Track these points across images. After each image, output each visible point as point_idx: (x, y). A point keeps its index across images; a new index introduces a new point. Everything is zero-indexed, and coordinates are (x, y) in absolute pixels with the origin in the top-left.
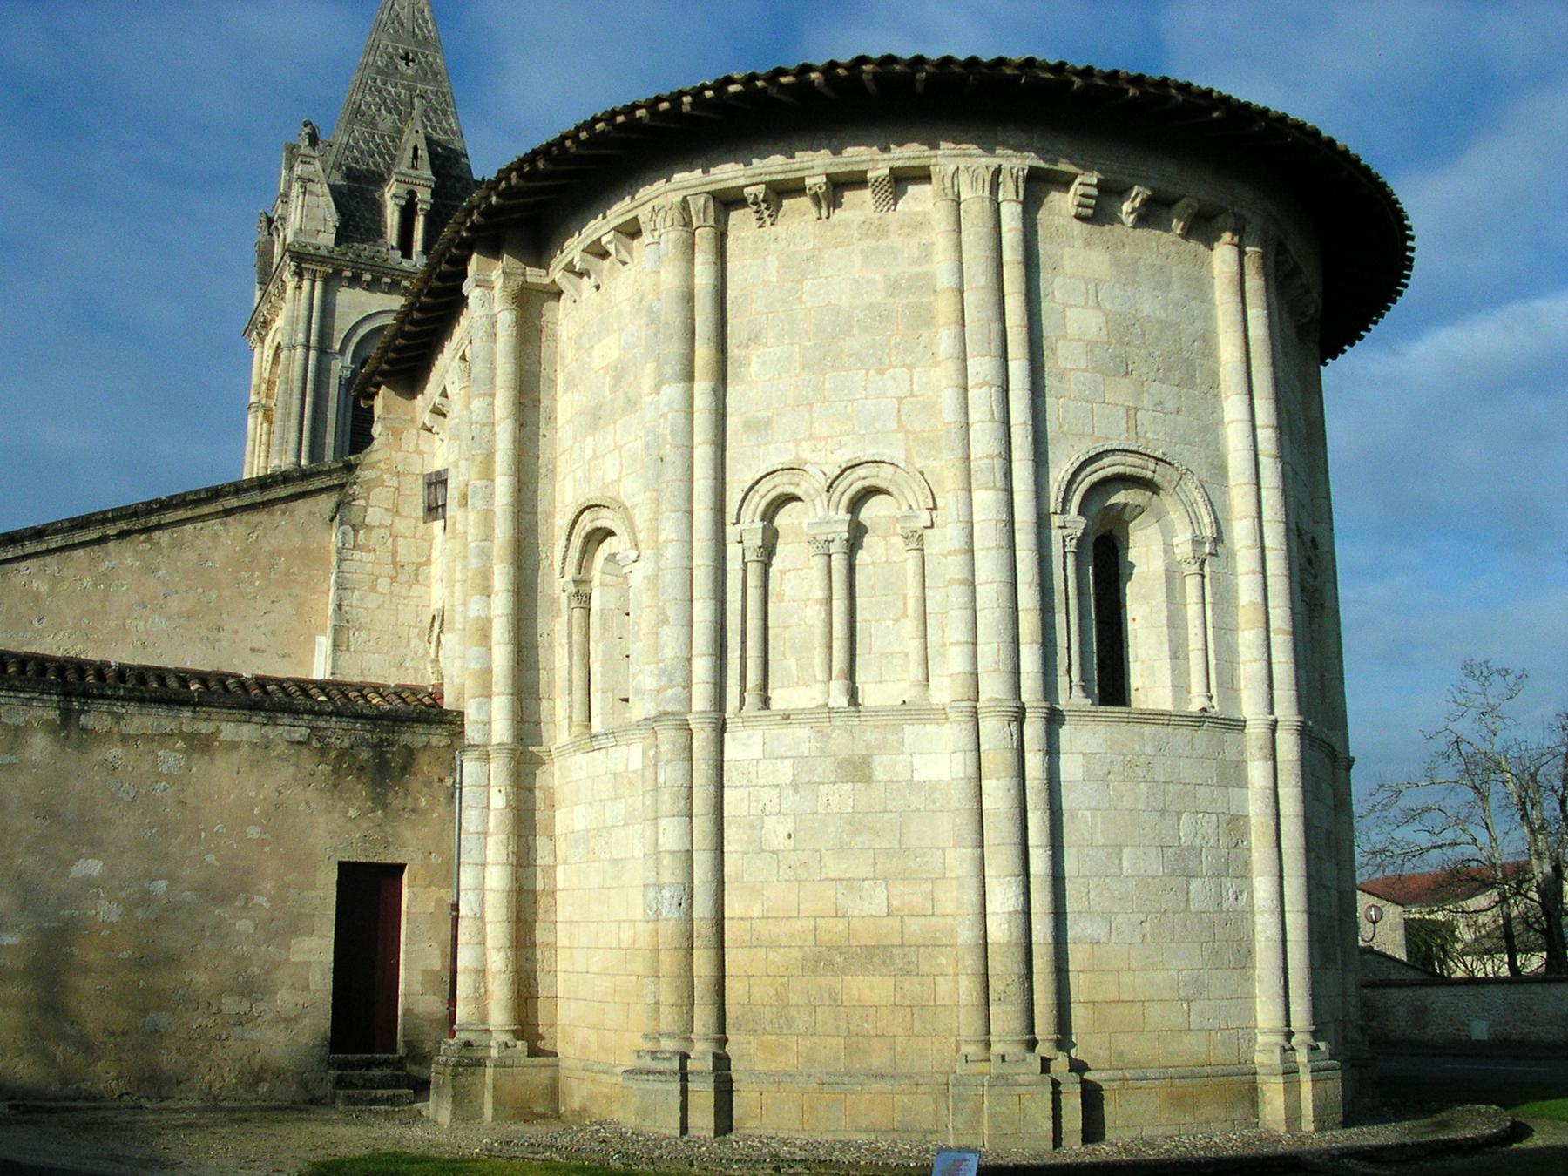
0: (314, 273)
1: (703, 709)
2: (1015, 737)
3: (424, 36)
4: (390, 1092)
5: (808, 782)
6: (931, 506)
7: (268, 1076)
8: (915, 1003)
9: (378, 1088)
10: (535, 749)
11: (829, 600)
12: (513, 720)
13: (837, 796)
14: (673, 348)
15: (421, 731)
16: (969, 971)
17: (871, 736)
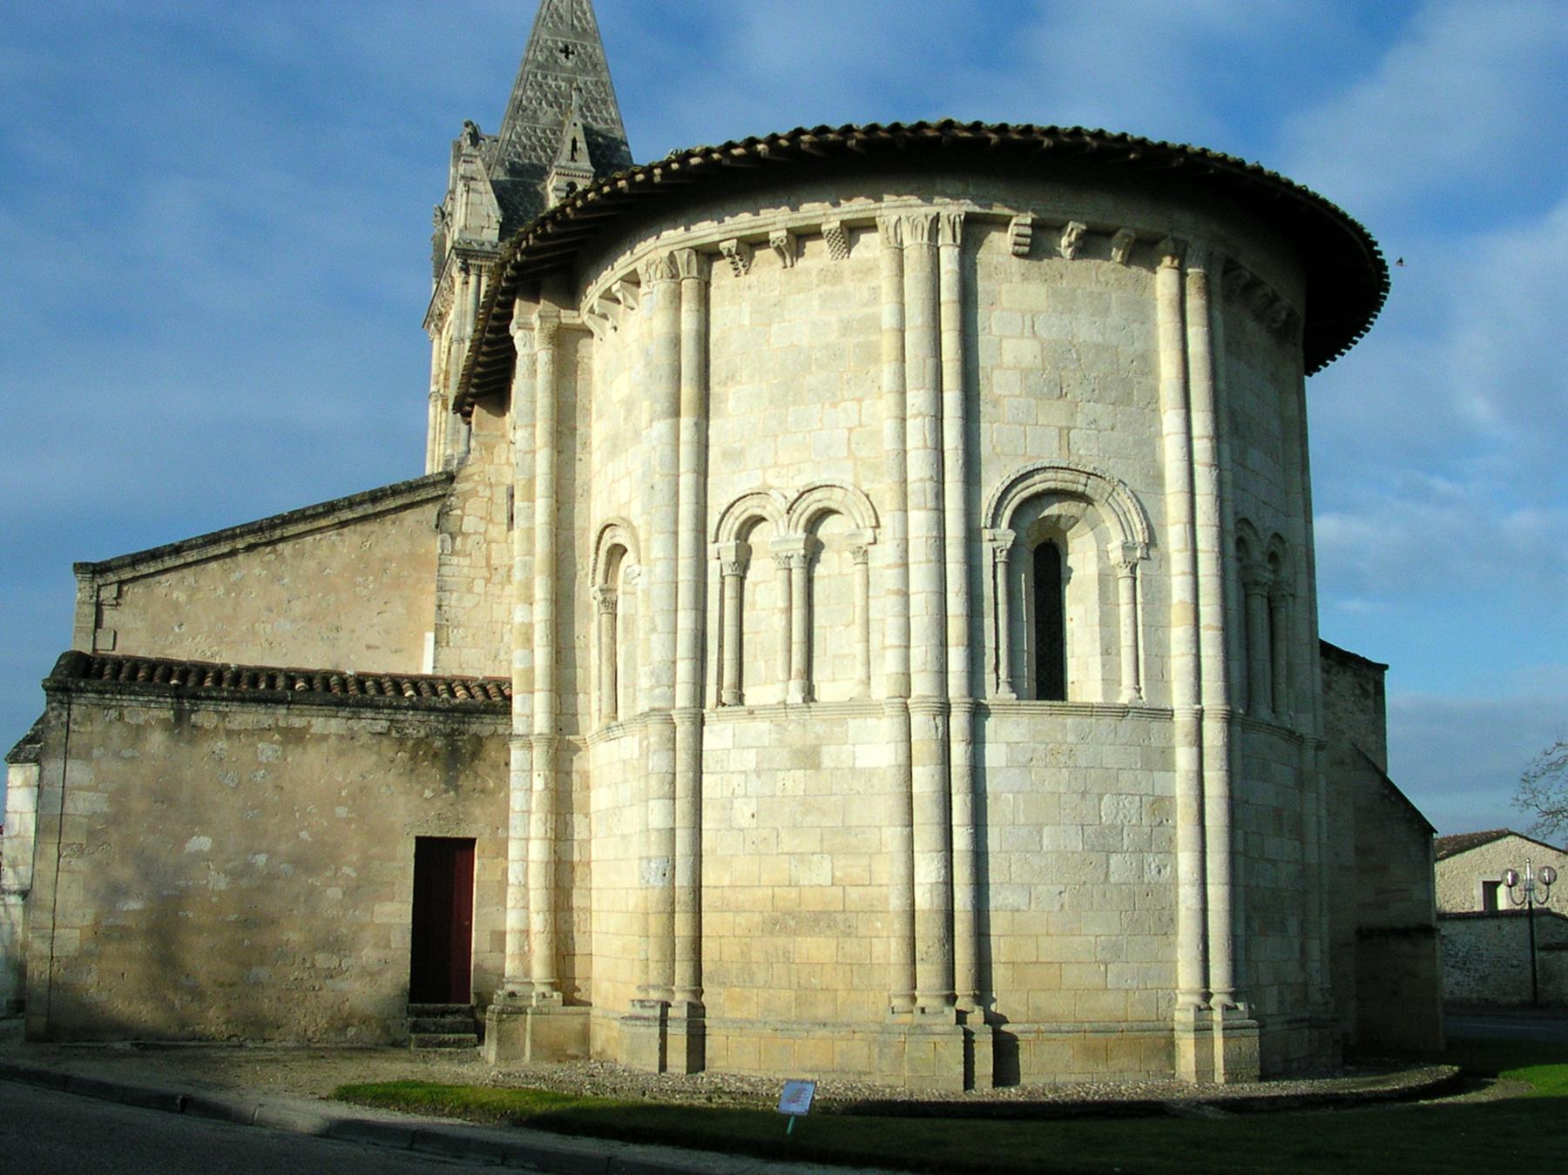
0: (480, 267)
1: (684, 705)
2: (940, 729)
3: (582, 28)
4: (457, 1036)
5: (769, 769)
6: (874, 524)
7: (356, 1021)
8: (854, 961)
9: (449, 1033)
10: (571, 738)
11: (790, 608)
12: (551, 713)
13: (791, 781)
14: (663, 388)
15: (489, 721)
17: (820, 729)
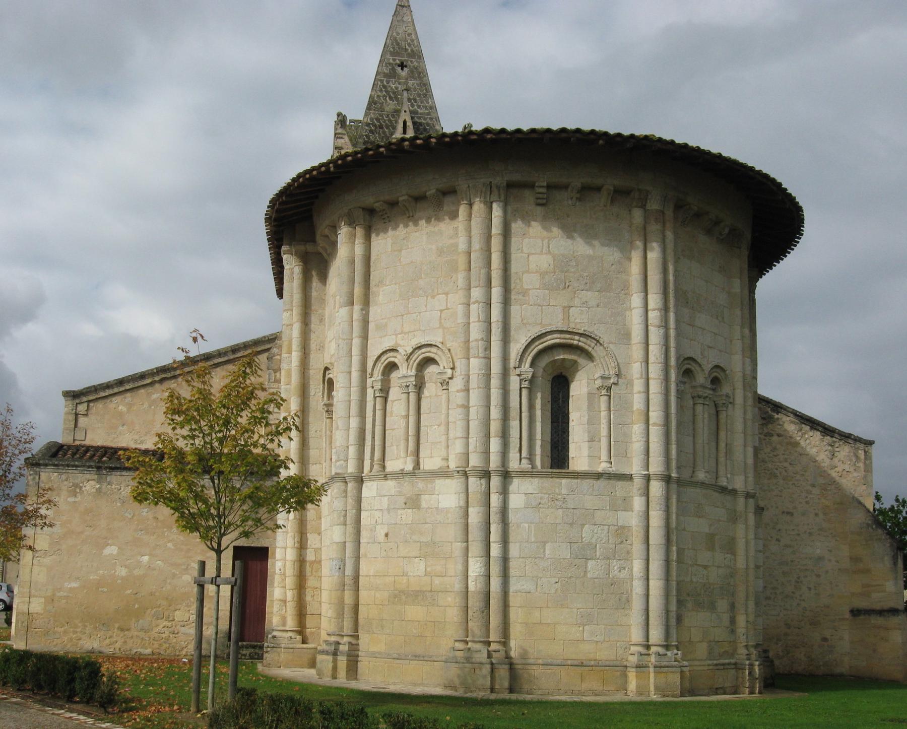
16: (457, 605)
